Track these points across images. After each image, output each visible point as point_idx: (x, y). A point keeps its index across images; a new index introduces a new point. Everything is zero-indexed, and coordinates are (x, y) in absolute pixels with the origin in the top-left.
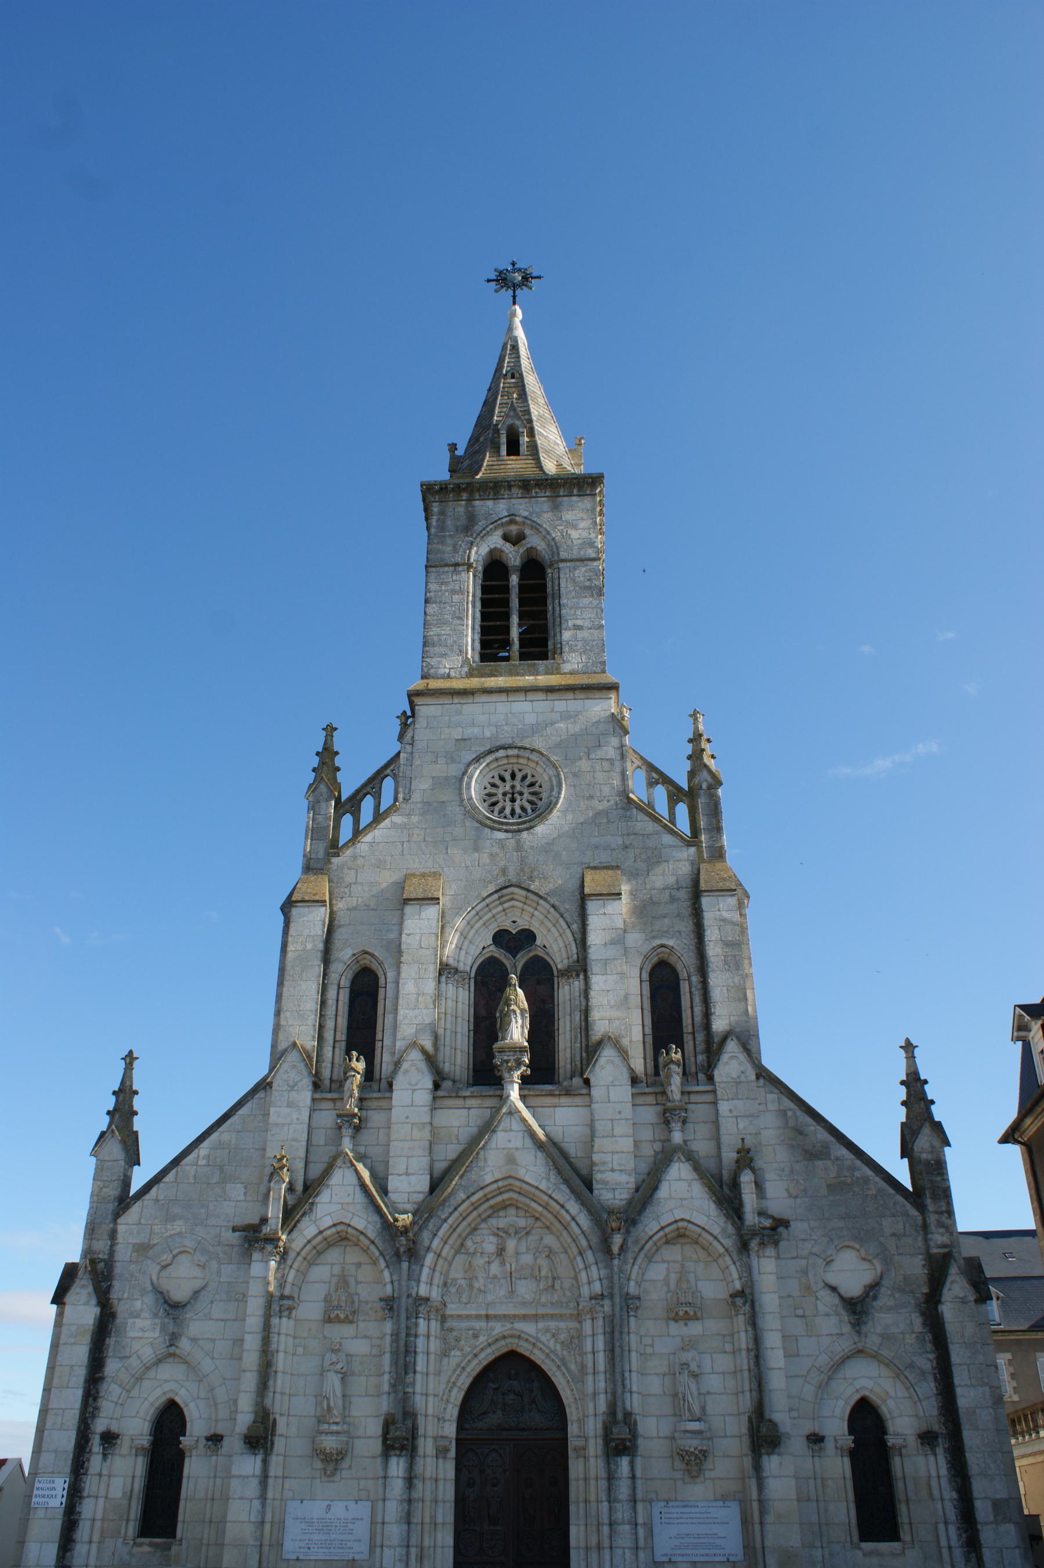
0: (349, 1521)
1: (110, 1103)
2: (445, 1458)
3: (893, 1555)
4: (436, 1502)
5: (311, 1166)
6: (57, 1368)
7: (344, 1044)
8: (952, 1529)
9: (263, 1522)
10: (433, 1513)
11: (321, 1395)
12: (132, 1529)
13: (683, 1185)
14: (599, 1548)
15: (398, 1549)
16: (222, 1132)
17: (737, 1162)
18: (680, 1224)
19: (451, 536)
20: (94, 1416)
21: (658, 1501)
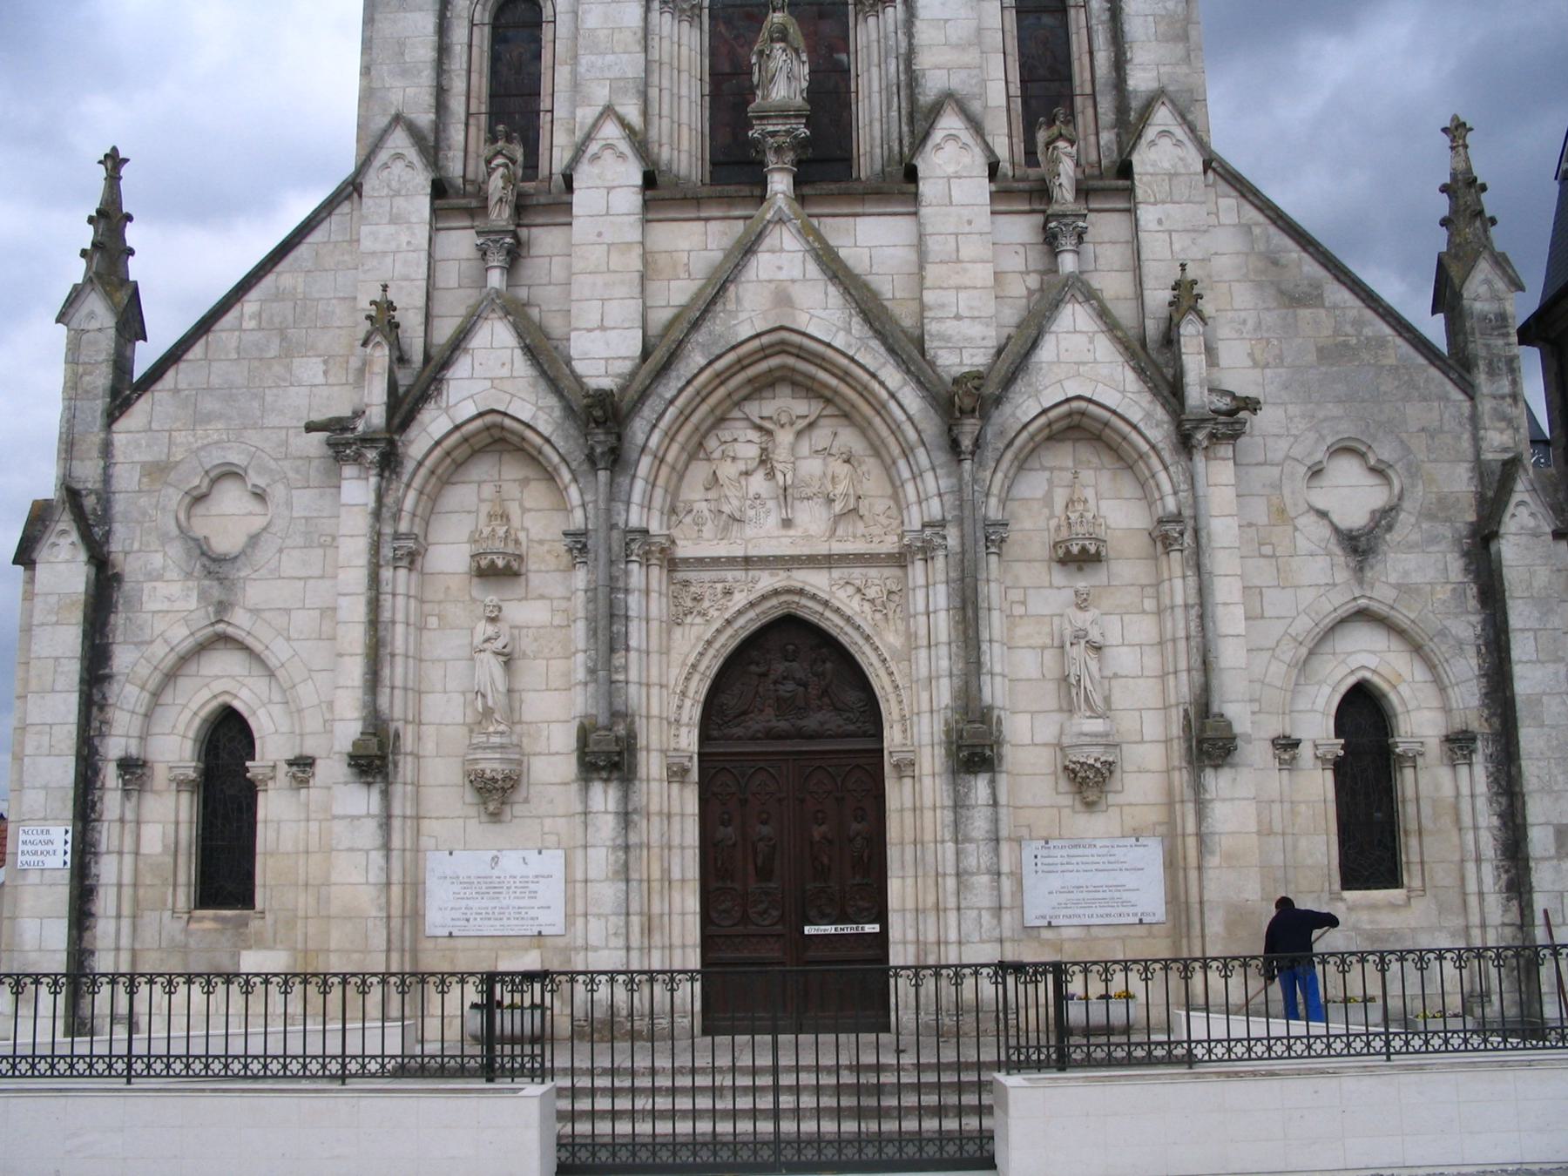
0: (531, 879)
1: (86, 237)
2: (682, 782)
3: (1393, 906)
4: (670, 848)
5: (436, 323)
6: (33, 663)
7: (483, 118)
8: (1488, 871)
9: (388, 884)
10: (666, 865)
12: (184, 897)
13: (1082, 340)
15: (613, 919)
16: (279, 274)
17: (1171, 304)
18: (1075, 405)
21: (1031, 839)
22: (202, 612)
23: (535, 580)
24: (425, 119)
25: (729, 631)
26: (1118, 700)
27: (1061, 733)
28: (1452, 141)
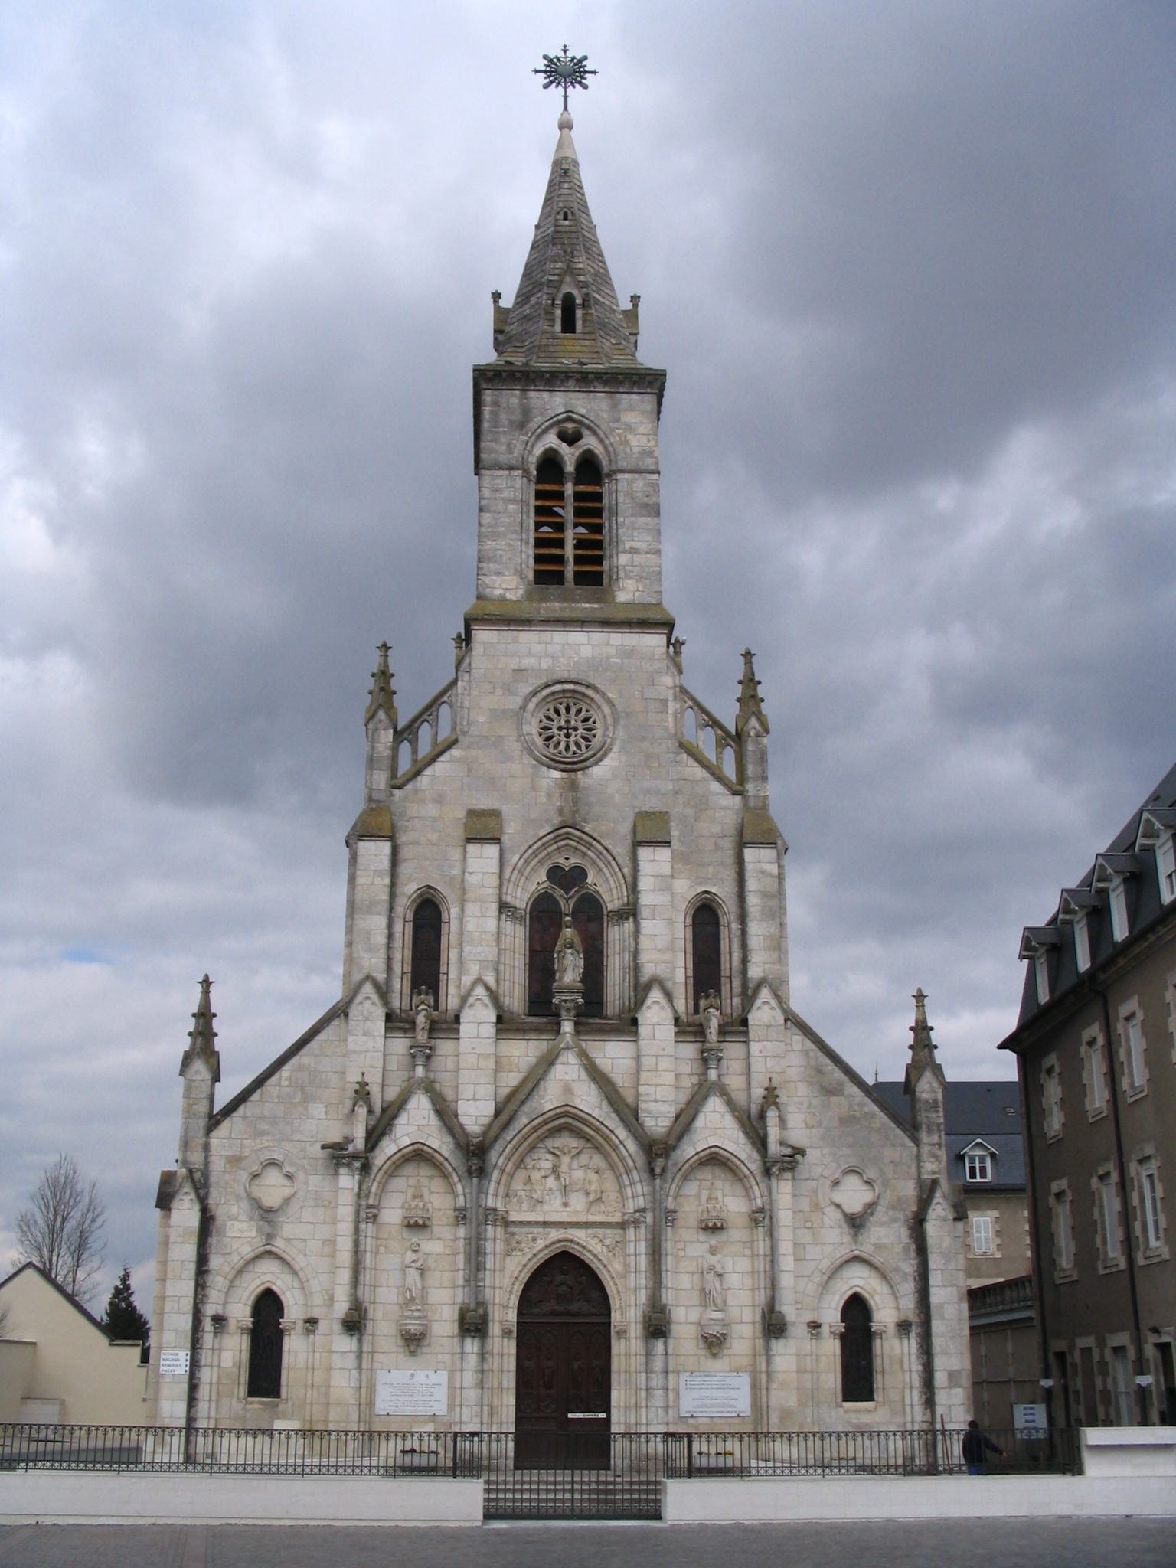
3: (868, 1411)
4: (502, 1371)
6: (169, 1263)
9: (360, 1387)
11: (404, 1286)
12: (243, 1390)
14: (637, 1407)
17: (764, 1097)
18: (713, 1150)
19: (505, 432)
20: (203, 1302)
22: (259, 1239)
23: (436, 1229)
24: (381, 977)
25: (535, 1260)
26: (730, 1302)
27: (701, 1318)
28: (917, 1002)
